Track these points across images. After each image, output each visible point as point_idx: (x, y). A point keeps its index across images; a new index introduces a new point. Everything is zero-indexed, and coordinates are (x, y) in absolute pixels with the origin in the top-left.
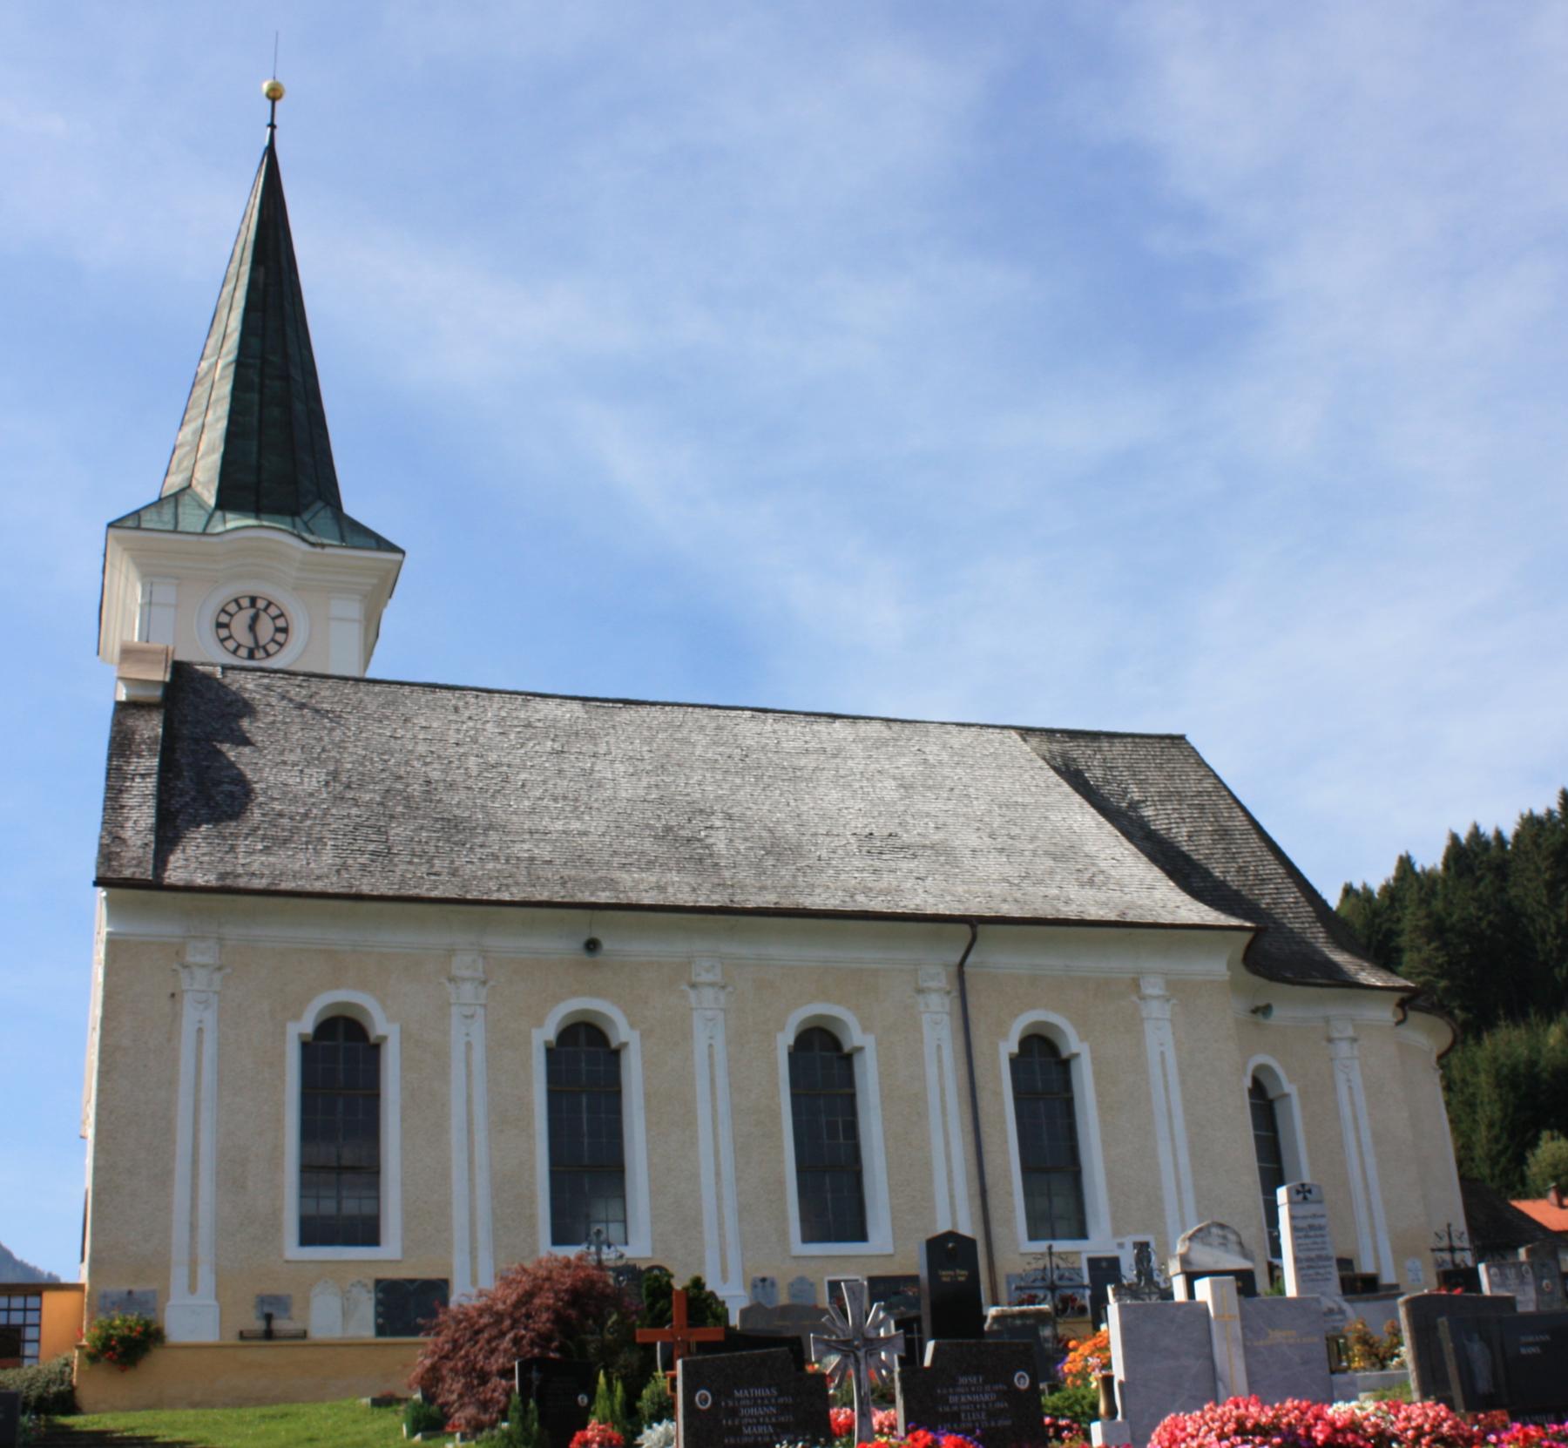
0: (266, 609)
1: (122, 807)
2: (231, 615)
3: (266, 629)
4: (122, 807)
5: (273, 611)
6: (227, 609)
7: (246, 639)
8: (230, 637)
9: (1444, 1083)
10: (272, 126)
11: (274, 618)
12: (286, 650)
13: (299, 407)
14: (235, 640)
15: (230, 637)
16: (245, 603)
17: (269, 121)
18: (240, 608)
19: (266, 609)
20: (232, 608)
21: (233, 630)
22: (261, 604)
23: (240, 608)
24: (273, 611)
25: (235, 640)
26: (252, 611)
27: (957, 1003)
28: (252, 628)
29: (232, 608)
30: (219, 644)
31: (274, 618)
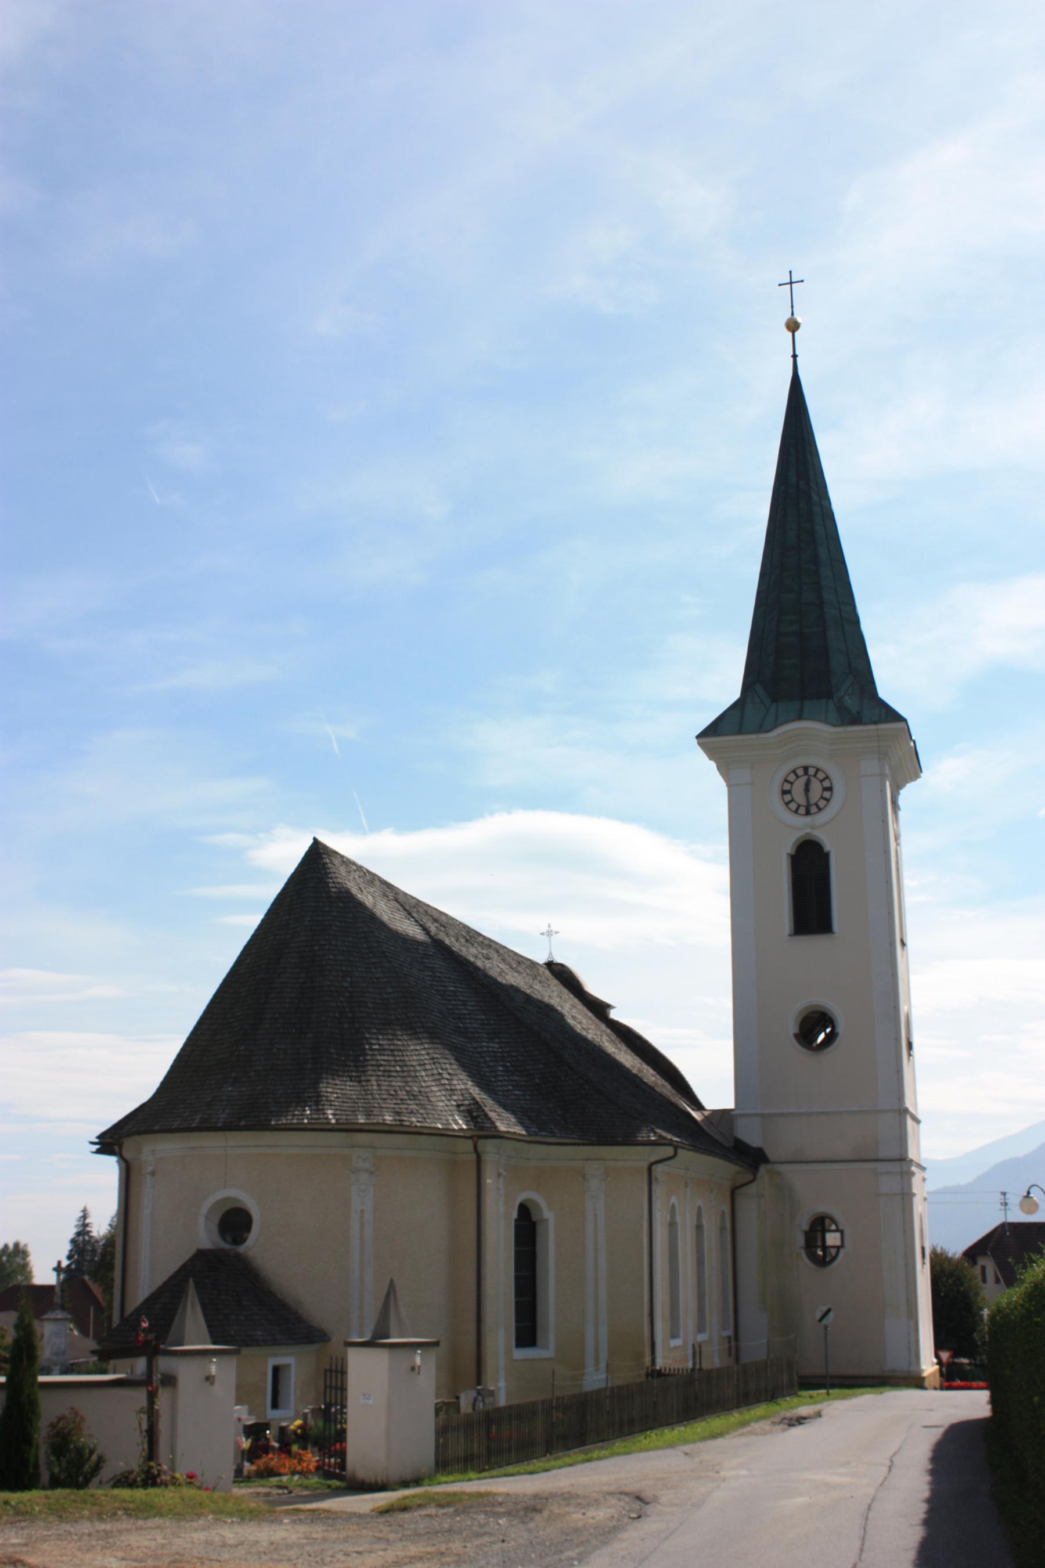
0: (815, 775)
1: (686, 1186)
2: (792, 783)
3: (816, 788)
4: (686, 1186)
5: (821, 775)
6: (788, 779)
7: (800, 799)
8: (792, 800)
9: (28, 1269)
10: (795, 356)
11: (821, 781)
12: (836, 789)
13: (823, 553)
14: (795, 780)
15: (792, 800)
16: (800, 772)
17: (792, 354)
18: (798, 777)
19: (815, 775)
20: (792, 778)
21: (796, 782)
22: (812, 771)
23: (798, 777)
24: (821, 775)
25: (795, 780)
26: (806, 778)
27: (726, 1208)
28: (807, 789)
29: (792, 778)
30: (783, 780)
31: (821, 781)
